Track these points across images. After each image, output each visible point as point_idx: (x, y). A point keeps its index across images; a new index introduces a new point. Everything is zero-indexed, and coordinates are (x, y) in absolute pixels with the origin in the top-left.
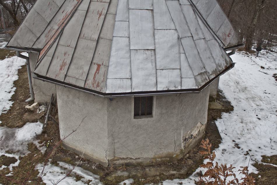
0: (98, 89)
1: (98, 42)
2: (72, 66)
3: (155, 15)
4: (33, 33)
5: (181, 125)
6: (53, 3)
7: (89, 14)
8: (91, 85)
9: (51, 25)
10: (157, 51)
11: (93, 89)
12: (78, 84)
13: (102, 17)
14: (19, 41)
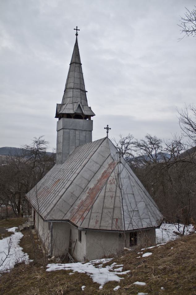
0: (119, 230)
1: (114, 209)
2: (102, 222)
3: (135, 196)
4: (62, 212)
5: (183, 197)
6: (74, 195)
7: (105, 198)
8: (115, 228)
9: (73, 206)
10: (139, 211)
11: (117, 230)
12: (108, 229)
13: (113, 198)
14: (53, 216)
